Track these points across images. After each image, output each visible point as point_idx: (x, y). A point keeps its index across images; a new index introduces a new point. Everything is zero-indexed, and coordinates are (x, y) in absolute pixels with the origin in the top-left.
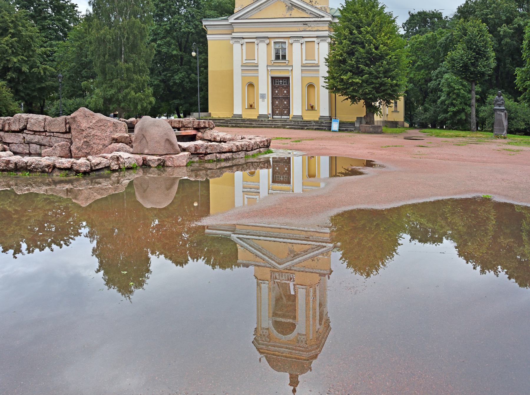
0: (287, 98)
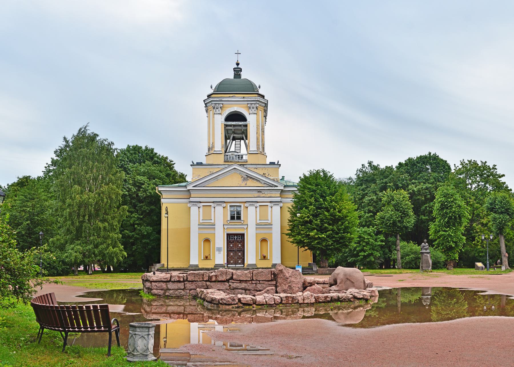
0: (242, 251)
